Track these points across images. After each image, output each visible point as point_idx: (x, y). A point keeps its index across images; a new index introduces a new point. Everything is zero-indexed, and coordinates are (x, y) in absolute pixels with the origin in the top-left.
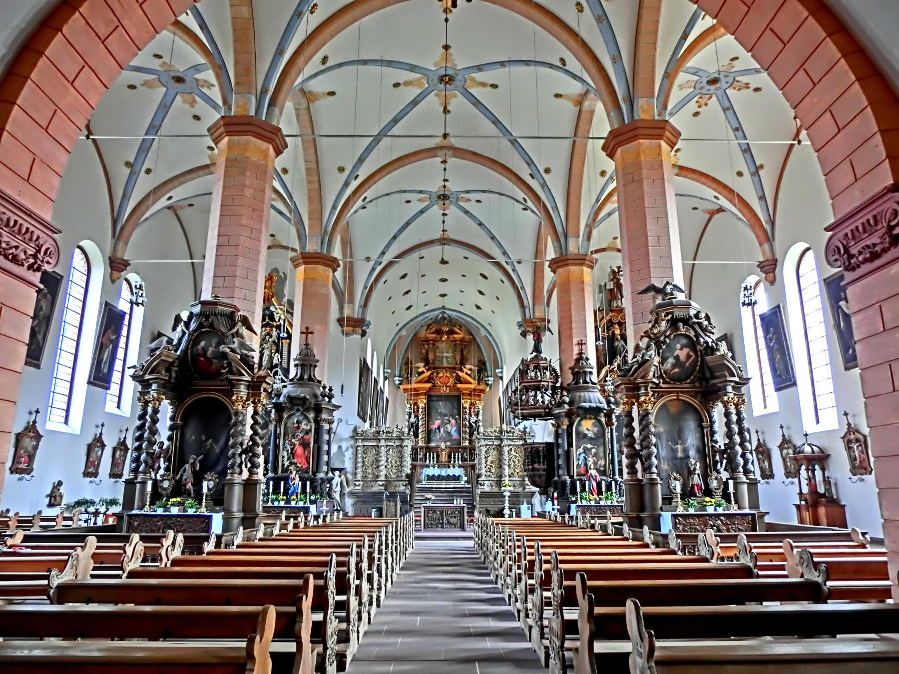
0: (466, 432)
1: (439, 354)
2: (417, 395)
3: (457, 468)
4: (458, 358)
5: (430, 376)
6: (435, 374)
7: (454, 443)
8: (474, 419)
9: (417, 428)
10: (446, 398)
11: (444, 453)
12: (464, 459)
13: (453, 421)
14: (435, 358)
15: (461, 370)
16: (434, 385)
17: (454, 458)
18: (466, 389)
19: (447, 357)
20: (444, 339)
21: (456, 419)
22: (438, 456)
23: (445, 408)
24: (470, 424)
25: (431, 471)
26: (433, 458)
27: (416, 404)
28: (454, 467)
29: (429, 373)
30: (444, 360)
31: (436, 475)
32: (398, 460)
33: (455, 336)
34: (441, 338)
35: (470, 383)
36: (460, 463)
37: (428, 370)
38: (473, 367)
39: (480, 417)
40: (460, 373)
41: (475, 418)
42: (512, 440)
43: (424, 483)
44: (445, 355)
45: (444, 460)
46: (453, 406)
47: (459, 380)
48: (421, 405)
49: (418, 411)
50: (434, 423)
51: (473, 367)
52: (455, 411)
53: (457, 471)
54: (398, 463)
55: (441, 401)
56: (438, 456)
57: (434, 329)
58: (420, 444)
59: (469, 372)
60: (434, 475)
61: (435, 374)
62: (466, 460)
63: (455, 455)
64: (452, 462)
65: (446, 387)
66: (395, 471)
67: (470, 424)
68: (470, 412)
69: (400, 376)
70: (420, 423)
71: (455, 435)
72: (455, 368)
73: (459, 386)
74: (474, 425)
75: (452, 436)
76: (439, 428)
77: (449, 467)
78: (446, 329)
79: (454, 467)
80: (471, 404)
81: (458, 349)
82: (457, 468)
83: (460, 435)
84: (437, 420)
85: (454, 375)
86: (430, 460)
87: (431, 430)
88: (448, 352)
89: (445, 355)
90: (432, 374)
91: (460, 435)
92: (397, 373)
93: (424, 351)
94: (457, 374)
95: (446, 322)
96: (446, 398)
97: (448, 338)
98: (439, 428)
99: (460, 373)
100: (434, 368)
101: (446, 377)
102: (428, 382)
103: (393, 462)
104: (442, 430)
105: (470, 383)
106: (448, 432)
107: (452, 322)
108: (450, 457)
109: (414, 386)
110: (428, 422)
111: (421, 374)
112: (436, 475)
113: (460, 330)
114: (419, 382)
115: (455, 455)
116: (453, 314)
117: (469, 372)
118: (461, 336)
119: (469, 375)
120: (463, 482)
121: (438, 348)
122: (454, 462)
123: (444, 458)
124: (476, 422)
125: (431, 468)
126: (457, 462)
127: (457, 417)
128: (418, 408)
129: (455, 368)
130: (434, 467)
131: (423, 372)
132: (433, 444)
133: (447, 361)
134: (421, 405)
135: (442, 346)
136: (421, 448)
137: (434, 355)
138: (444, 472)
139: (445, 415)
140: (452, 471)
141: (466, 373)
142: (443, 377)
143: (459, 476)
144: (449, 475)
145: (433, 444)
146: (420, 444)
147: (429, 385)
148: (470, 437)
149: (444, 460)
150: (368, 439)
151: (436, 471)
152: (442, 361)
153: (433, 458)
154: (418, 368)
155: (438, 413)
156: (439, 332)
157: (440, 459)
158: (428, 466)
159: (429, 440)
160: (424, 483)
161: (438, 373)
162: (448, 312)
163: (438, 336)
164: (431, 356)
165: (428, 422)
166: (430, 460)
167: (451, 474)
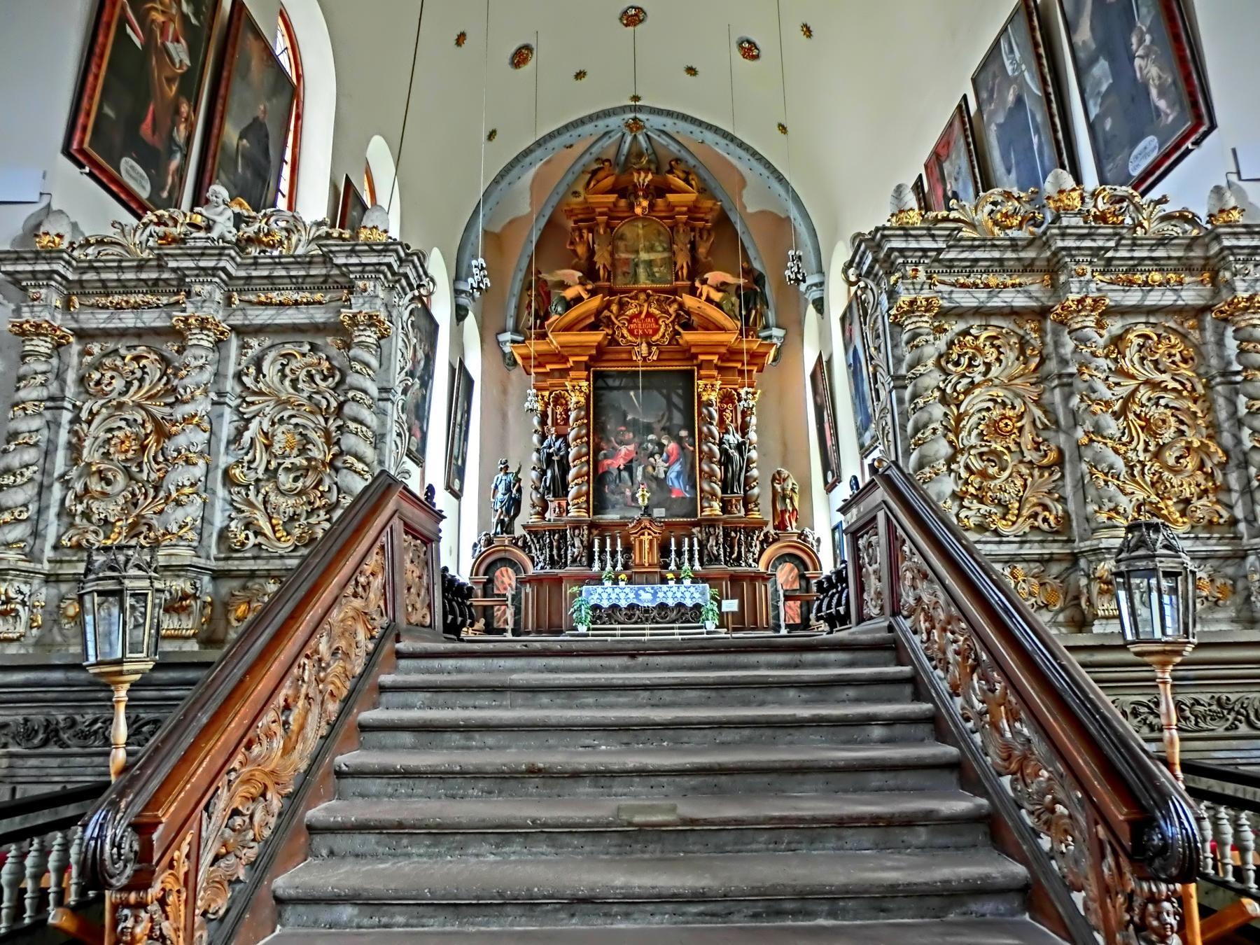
0: (711, 475)
1: (623, 256)
2: (564, 373)
3: (687, 582)
4: (683, 261)
5: (598, 312)
6: (614, 308)
7: (676, 509)
8: (733, 438)
9: (565, 468)
10: (652, 378)
11: (646, 538)
12: (708, 558)
13: (672, 446)
14: (613, 265)
15: (693, 291)
16: (613, 341)
17: (679, 554)
18: (710, 348)
19: (650, 264)
20: (638, 210)
21: (679, 440)
22: (628, 549)
23: (646, 406)
24: (724, 452)
25: (605, 595)
26: (613, 554)
27: (558, 400)
28: (679, 581)
29: (596, 302)
30: (641, 271)
31: (623, 604)
32: (313, 426)
33: (671, 197)
34: (631, 207)
35: (721, 328)
36: (697, 567)
37: (593, 293)
38: (729, 279)
39: (753, 436)
40: (689, 301)
41: (738, 436)
42: (1128, 274)
43: (582, 629)
44: (644, 256)
45: (646, 561)
46: (670, 404)
47: (686, 321)
48: (575, 399)
49: (566, 421)
50: (614, 454)
51: (729, 279)
52: (678, 418)
53: (690, 593)
54: (319, 452)
55: (636, 388)
56: (628, 549)
57: (609, 181)
58: (573, 512)
59: (716, 296)
60: (615, 607)
61: (614, 308)
62: (715, 559)
63: (679, 544)
64: (673, 567)
65: (649, 345)
66: (286, 505)
67: (724, 452)
68: (722, 421)
69: (516, 331)
70: (573, 452)
71: (678, 488)
72: (674, 291)
73: (688, 337)
74: (736, 455)
75: (670, 491)
76: (629, 468)
77: (664, 580)
78: (645, 179)
79: (679, 581)
80: (727, 398)
81: (682, 241)
82: (687, 582)
83: (694, 487)
84: (621, 443)
85: (672, 309)
86: (603, 561)
87: (607, 472)
88: (651, 249)
89: (644, 256)
90: (607, 306)
91: (694, 487)
92: (510, 323)
93: (581, 250)
94: (681, 306)
95: (644, 160)
96: (652, 378)
97: (652, 206)
98: (629, 468)
99: (689, 301)
100: (612, 292)
101: (649, 315)
102: (594, 327)
103: (281, 438)
104: (639, 472)
105: (721, 328)
106: (656, 478)
107: (663, 165)
108: (664, 550)
109: (555, 341)
110: (597, 450)
111: (569, 305)
112: (623, 604)
113: (687, 181)
114: (568, 328)
115: (679, 544)
116: (669, 124)
117: (716, 296)
118: (691, 197)
119: (719, 306)
120: (710, 626)
121: (622, 237)
122: (679, 567)
123: (647, 555)
124: (740, 447)
125: (608, 584)
126: (686, 565)
127: (683, 433)
128: (567, 411)
129: (674, 291)
130: (616, 582)
131: (578, 299)
132: (612, 516)
133: (651, 275)
134: (575, 399)
135: (635, 232)
136: (577, 525)
137: (612, 254)
138: (646, 597)
139: (649, 429)
140: (671, 594)
141: (709, 300)
142: (637, 316)
143: (697, 607)
144: (663, 606)
145: (612, 516)
146: (573, 512)
147: (596, 337)
148: (724, 491)
149: (646, 561)
150: (105, 288)
151: (623, 595)
152: (636, 274)
153: (613, 554)
154: (563, 285)
155: (625, 423)
156: (624, 191)
157: (636, 557)
158: (599, 581)
159: (600, 505)
160: (582, 629)
161: (622, 306)
162: (656, 121)
163: (623, 203)
164: (601, 260)
165: (597, 450)
166: (603, 561)
167: (671, 602)
